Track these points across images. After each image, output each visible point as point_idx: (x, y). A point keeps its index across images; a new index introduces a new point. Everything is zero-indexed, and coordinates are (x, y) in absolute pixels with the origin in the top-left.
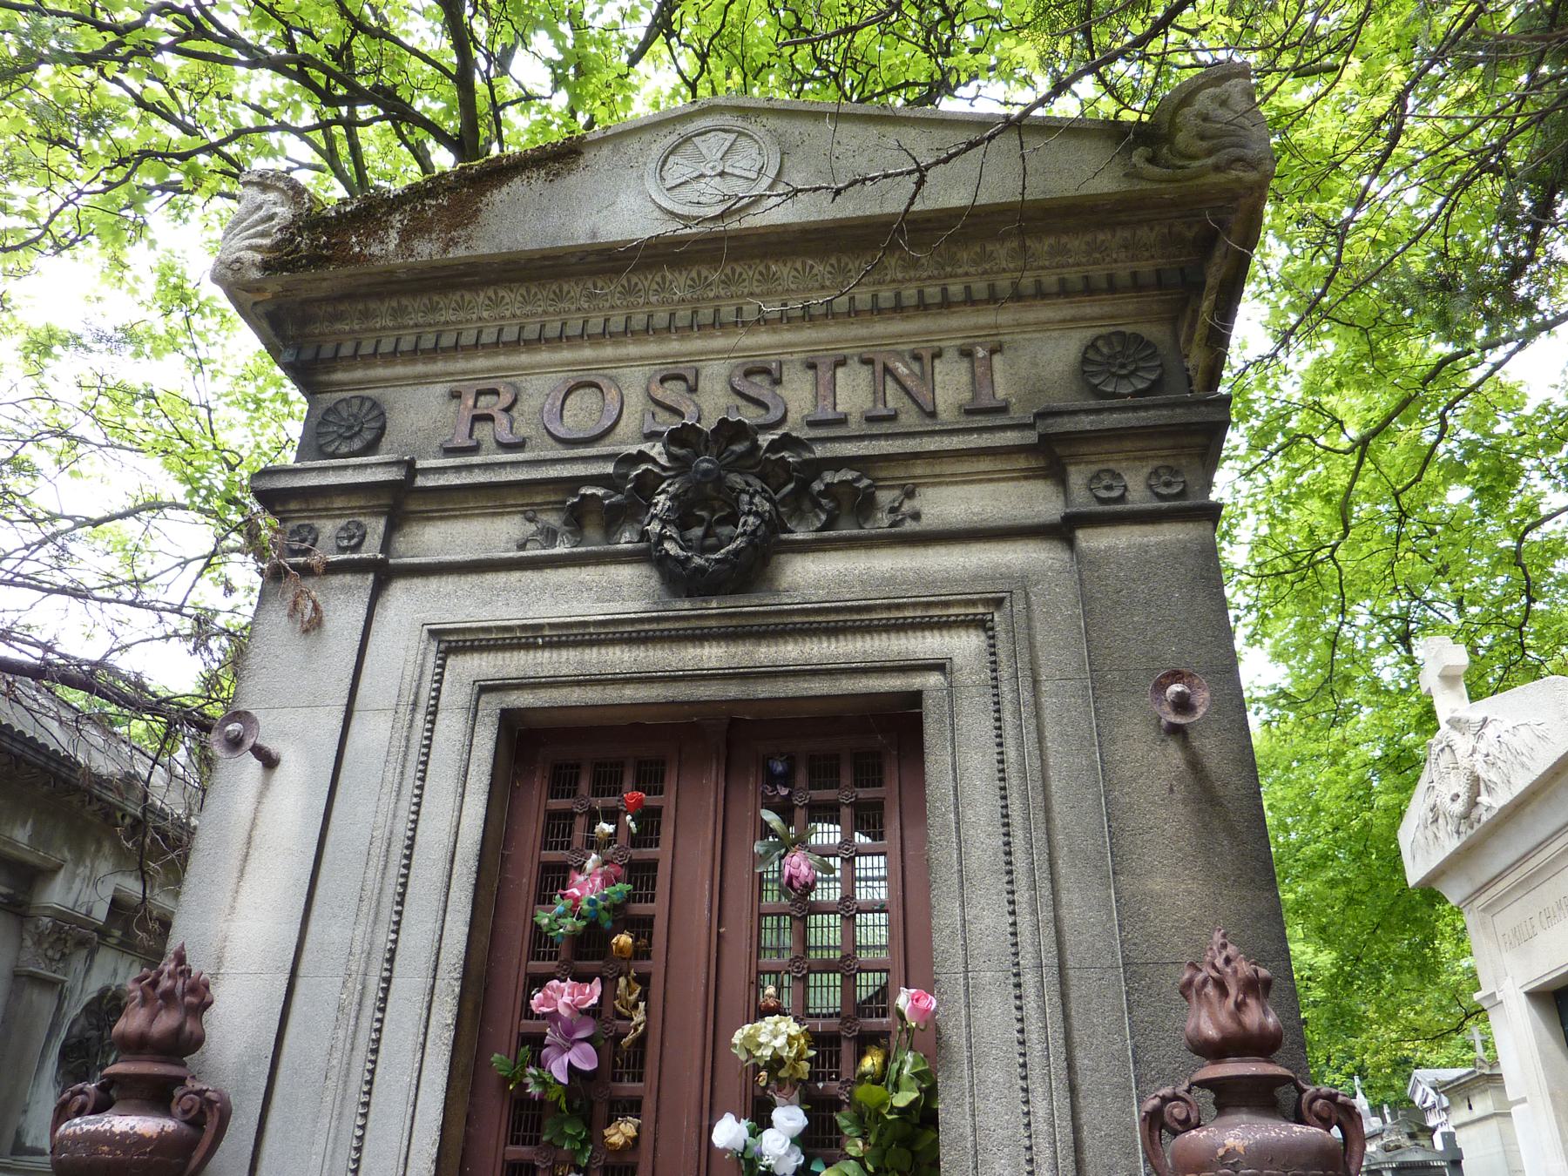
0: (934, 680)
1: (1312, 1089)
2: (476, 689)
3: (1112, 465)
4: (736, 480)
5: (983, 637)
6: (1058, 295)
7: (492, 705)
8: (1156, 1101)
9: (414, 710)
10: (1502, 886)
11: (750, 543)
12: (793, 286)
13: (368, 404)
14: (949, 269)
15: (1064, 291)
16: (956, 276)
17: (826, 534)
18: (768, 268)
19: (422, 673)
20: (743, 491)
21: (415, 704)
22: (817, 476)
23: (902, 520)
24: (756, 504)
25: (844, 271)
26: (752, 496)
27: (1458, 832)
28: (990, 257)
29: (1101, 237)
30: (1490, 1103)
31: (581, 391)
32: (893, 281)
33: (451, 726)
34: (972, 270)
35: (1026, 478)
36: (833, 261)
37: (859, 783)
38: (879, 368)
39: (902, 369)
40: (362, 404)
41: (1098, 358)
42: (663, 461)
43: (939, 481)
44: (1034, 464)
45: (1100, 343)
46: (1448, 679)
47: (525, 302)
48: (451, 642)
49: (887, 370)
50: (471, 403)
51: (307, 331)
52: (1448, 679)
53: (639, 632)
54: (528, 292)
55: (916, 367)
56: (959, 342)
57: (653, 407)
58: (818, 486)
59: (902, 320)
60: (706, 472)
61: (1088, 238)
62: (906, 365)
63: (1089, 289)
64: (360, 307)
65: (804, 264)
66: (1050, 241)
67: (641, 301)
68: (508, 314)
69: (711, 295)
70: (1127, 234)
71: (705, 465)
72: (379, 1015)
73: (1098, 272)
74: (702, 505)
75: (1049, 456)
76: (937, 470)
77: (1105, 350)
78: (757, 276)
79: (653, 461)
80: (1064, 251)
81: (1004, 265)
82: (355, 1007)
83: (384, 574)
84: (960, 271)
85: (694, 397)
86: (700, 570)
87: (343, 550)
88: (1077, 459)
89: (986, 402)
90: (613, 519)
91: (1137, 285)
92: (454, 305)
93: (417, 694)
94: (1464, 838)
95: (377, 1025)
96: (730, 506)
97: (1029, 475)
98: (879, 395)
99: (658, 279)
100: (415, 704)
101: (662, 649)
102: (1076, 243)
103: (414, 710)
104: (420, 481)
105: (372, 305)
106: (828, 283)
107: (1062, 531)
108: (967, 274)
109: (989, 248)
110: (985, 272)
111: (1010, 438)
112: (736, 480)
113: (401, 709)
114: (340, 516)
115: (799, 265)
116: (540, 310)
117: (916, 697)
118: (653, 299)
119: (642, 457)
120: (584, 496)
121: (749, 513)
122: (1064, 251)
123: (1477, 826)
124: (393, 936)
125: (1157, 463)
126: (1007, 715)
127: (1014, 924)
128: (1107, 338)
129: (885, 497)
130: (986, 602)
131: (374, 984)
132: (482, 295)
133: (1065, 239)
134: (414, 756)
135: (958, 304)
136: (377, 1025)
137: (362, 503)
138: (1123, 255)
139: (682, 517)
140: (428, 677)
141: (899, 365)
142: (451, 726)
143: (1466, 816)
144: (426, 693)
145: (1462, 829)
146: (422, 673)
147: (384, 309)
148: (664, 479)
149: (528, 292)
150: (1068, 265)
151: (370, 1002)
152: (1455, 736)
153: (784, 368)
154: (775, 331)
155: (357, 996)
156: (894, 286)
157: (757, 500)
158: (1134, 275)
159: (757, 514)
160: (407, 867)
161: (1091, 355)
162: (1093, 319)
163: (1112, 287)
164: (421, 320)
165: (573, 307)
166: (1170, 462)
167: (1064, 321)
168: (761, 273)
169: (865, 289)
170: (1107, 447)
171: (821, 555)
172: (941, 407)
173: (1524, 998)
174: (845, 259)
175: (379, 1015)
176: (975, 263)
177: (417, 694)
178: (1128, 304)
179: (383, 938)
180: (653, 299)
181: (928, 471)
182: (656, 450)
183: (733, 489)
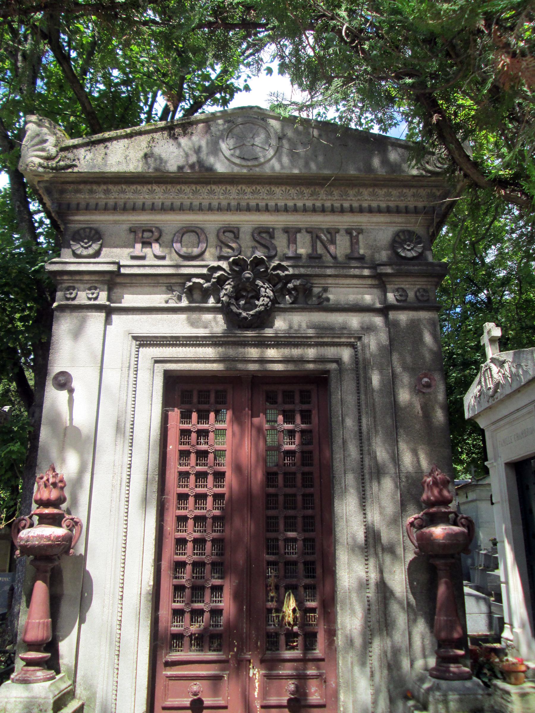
0: (334, 366)
1: (460, 515)
2: (153, 362)
3: (402, 286)
4: (259, 283)
5: (353, 351)
6: (386, 213)
7: (160, 368)
8: (413, 519)
9: (129, 370)
10: (502, 423)
11: (265, 308)
12: (281, 198)
13: (93, 232)
14: (344, 197)
15: (388, 211)
16: (347, 200)
17: (293, 305)
18: (271, 189)
19: (130, 354)
20: (262, 287)
21: (129, 367)
22: (289, 282)
23: (323, 302)
24: (267, 291)
25: (302, 193)
26: (266, 289)
27: (488, 402)
28: (360, 194)
29: (405, 191)
30: (475, 495)
31: (188, 234)
32: (322, 199)
33: (144, 375)
34: (354, 199)
35: (370, 288)
36: (298, 189)
37: (302, 402)
38: (314, 236)
39: (323, 237)
40: (90, 232)
41: (400, 241)
42: (227, 269)
43: (337, 285)
44: (373, 283)
45: (400, 234)
46: (492, 340)
47: (165, 192)
48: (143, 341)
49: (318, 237)
50: (140, 235)
51: (63, 196)
52: (492, 340)
53: (219, 341)
54: (166, 188)
55: (329, 236)
56: (346, 227)
57: (220, 244)
58: (290, 285)
59: (324, 216)
60: (248, 278)
61: (400, 190)
62: (325, 236)
63: (398, 211)
64: (89, 187)
65: (286, 189)
66: (385, 190)
67: (216, 197)
68: (157, 197)
69: (246, 197)
70: (415, 191)
71: (248, 275)
72: (128, 488)
73: (402, 205)
74: (245, 292)
75: (380, 282)
76: (337, 282)
77: (402, 237)
78: (266, 192)
79: (223, 270)
80: (390, 195)
81: (366, 198)
82: (119, 485)
83: (109, 312)
84: (349, 198)
85: (238, 241)
86: (245, 318)
87: (90, 299)
88: (390, 283)
89: (356, 255)
90: (205, 294)
91: (416, 211)
92: (132, 191)
93: (129, 363)
94: (490, 404)
95: (127, 492)
96: (256, 291)
97: (372, 286)
98: (314, 247)
99: (224, 188)
100: (129, 367)
101: (229, 348)
102: (394, 192)
103: (129, 370)
104: (123, 271)
105: (95, 187)
106: (295, 198)
107: (385, 310)
108: (351, 200)
109: (361, 190)
110: (359, 200)
111: (366, 272)
112: (259, 283)
113: (124, 369)
114: (86, 283)
115: (284, 189)
116: (171, 197)
117: (328, 372)
118: (221, 197)
119: (219, 268)
120: (194, 283)
121: (265, 296)
122: (390, 195)
123: (496, 400)
124: (130, 459)
125: (419, 287)
126: (362, 382)
127: (362, 458)
128: (403, 232)
129: (316, 290)
130: (355, 338)
131: (125, 477)
132: (145, 187)
133: (390, 190)
134: (131, 389)
135: (347, 212)
136: (127, 492)
137: (97, 278)
138: (412, 199)
139: (237, 295)
140: (133, 356)
141: (322, 235)
142: (144, 375)
143: (492, 396)
144: (133, 363)
145: (490, 401)
146: (130, 354)
147: (100, 189)
148: (228, 279)
149: (166, 188)
150: (391, 201)
151: (124, 484)
152: (492, 366)
153: (275, 231)
154: (271, 215)
155: (119, 482)
156: (321, 201)
157: (268, 290)
158: (415, 207)
159: (268, 297)
160: (132, 432)
161: (397, 239)
162: (398, 223)
163: (407, 211)
164: (117, 196)
165: (186, 197)
166: (424, 287)
167: (387, 223)
168: (268, 191)
169: (310, 202)
170: (402, 279)
171: (291, 313)
172: (339, 255)
173: (503, 465)
174: (303, 189)
175: (128, 488)
176: (355, 196)
177: (129, 363)
178: (412, 218)
179: (126, 460)
180: (221, 197)
181: (333, 282)
182: (224, 264)
183: (257, 285)
